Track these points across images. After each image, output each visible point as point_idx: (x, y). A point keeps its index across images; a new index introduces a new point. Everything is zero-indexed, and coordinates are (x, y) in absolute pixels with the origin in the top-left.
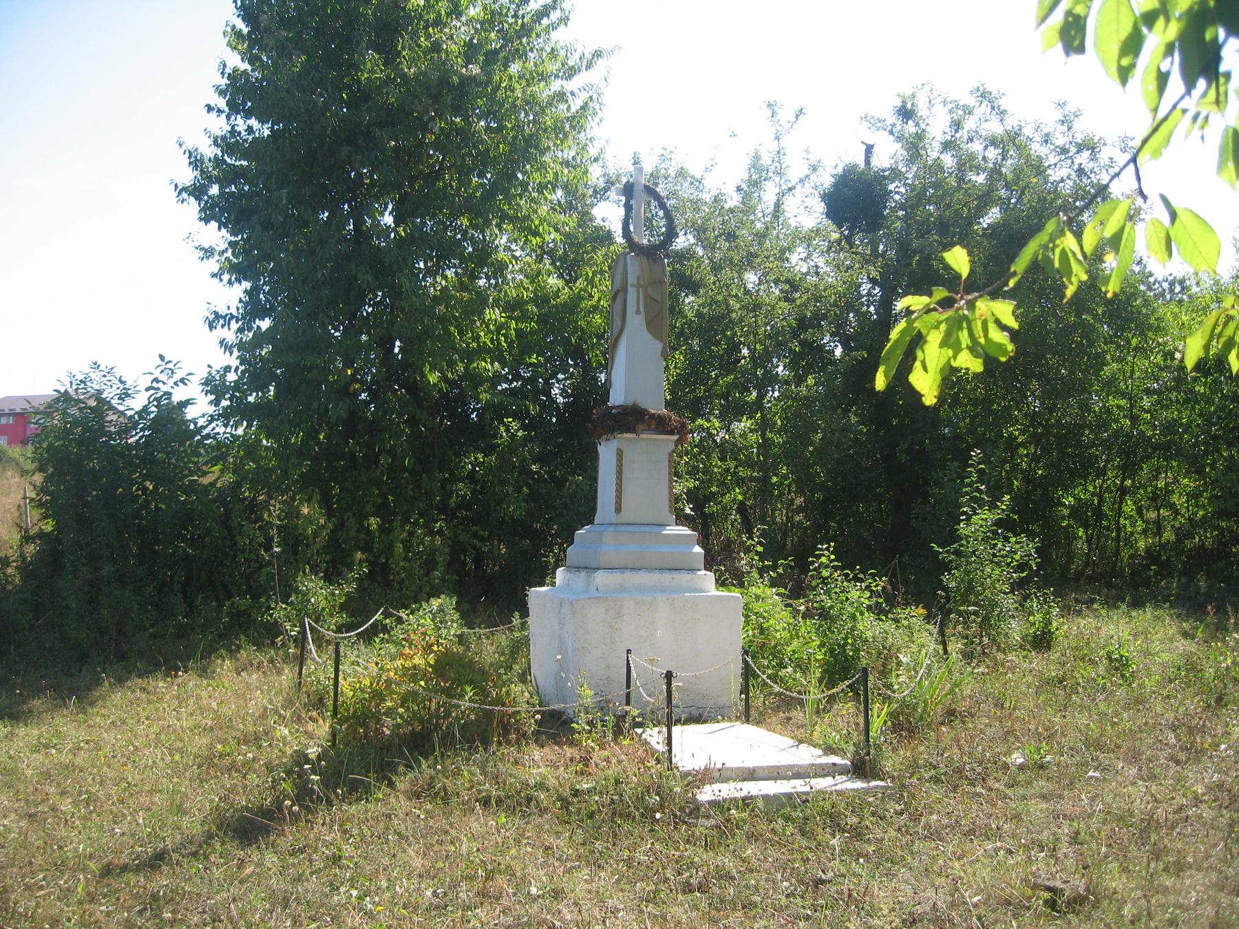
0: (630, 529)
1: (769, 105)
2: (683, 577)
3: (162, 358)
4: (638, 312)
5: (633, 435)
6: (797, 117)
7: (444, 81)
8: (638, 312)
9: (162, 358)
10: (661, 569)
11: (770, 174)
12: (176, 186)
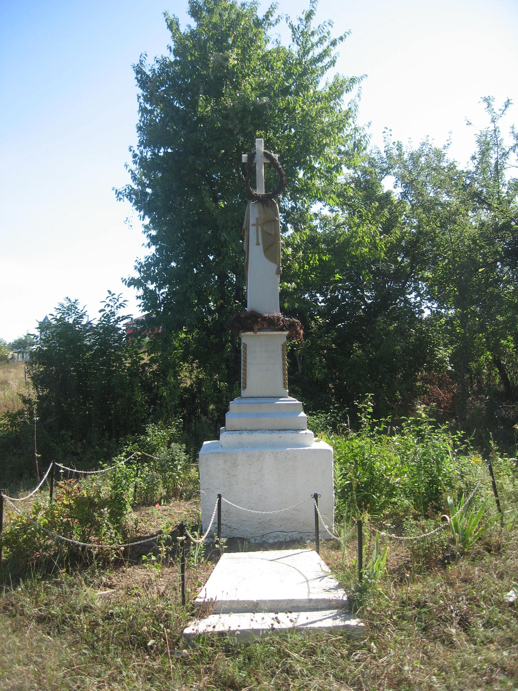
0: (251, 401)
1: (486, 100)
2: (288, 436)
3: (110, 292)
4: (258, 244)
5: (252, 333)
6: (506, 106)
7: (245, 109)
8: (258, 244)
9: (110, 292)
10: (272, 430)
11: (491, 146)
12: (116, 191)
